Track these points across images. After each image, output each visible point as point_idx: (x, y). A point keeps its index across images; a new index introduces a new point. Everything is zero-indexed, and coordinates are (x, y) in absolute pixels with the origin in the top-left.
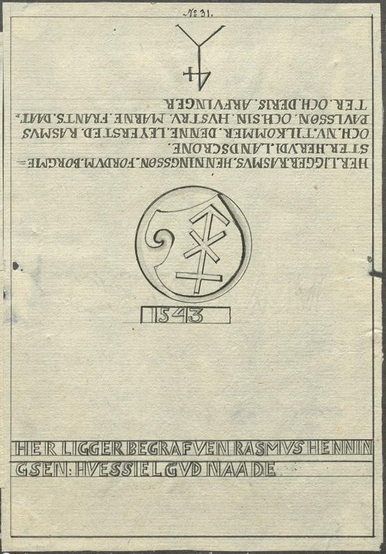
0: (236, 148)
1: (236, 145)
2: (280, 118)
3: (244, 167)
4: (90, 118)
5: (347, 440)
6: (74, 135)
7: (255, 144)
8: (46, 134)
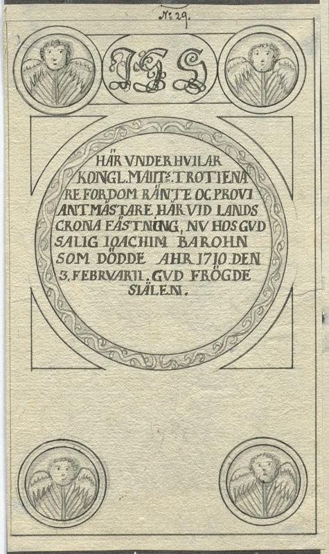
0: (119, 260)
1: (205, 214)
4: (144, 290)
6: (166, 159)
8: (95, 209)
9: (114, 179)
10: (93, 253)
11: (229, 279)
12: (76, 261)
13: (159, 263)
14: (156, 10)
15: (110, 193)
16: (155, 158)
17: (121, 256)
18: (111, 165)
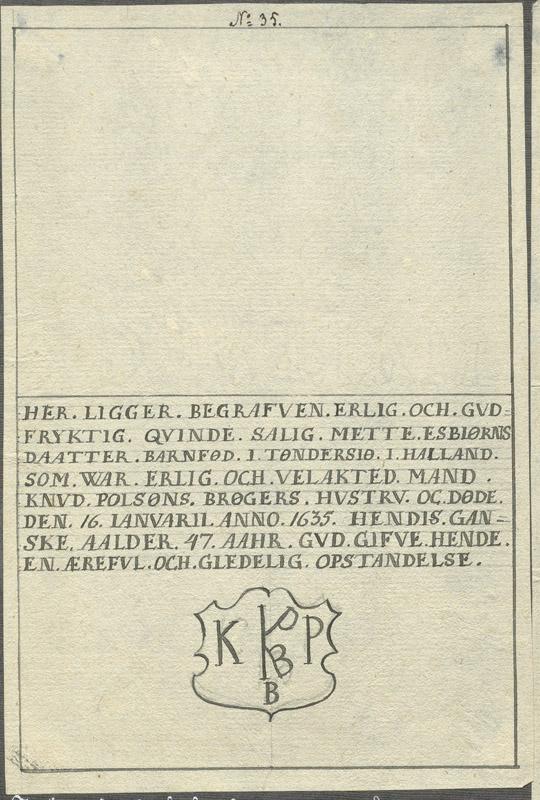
0: (477, 498)
2: (240, 479)
5: (264, 634)
11: (209, 567)
15: (310, 453)
16: (252, 558)
17: (455, 494)
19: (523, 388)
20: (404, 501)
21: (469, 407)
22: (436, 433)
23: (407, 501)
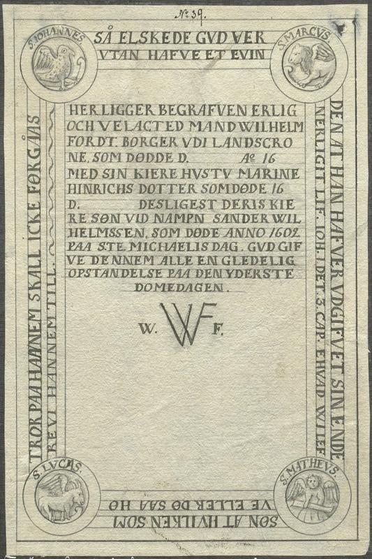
0: (204, 234)
3: (186, 291)
4: (200, 111)
7: (166, 264)
9: (132, 112)
10: (218, 206)
11: (132, 114)
12: (169, 235)
13: (226, 236)
14: (174, 9)
18: (30, 372)
19: (310, 318)
20: (153, 332)
21: (252, 246)
22: (168, 142)
23: (156, 332)
